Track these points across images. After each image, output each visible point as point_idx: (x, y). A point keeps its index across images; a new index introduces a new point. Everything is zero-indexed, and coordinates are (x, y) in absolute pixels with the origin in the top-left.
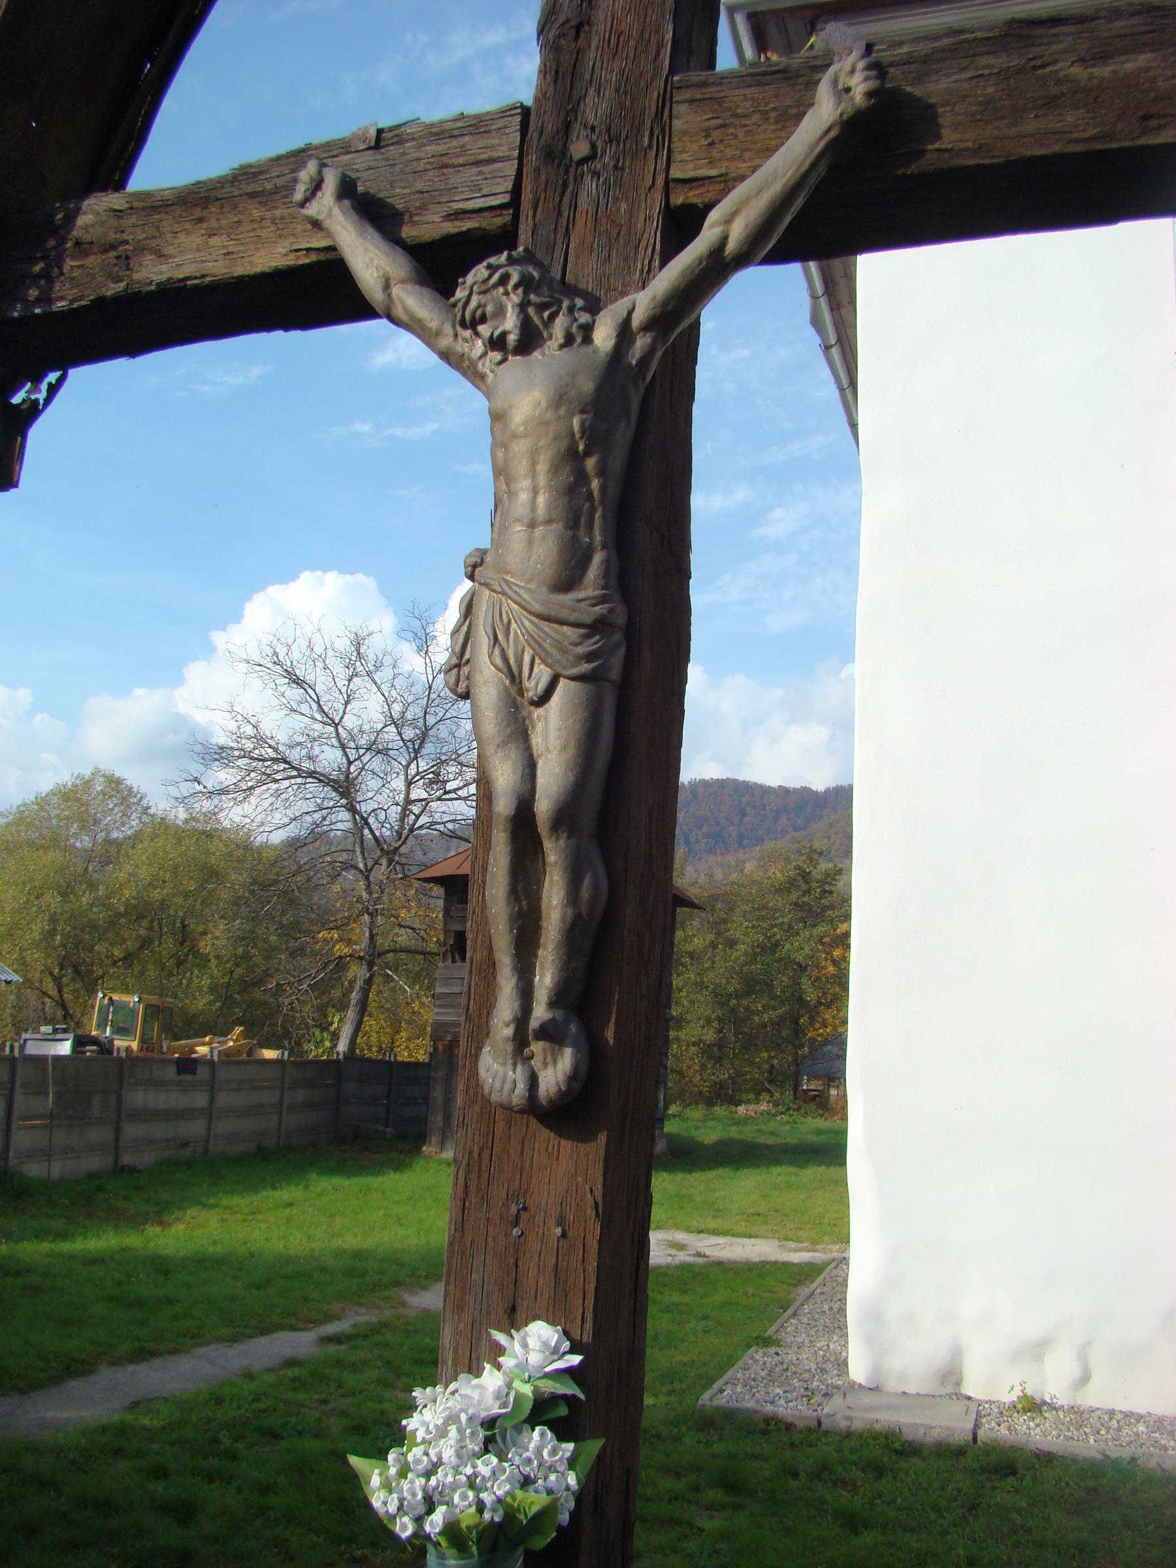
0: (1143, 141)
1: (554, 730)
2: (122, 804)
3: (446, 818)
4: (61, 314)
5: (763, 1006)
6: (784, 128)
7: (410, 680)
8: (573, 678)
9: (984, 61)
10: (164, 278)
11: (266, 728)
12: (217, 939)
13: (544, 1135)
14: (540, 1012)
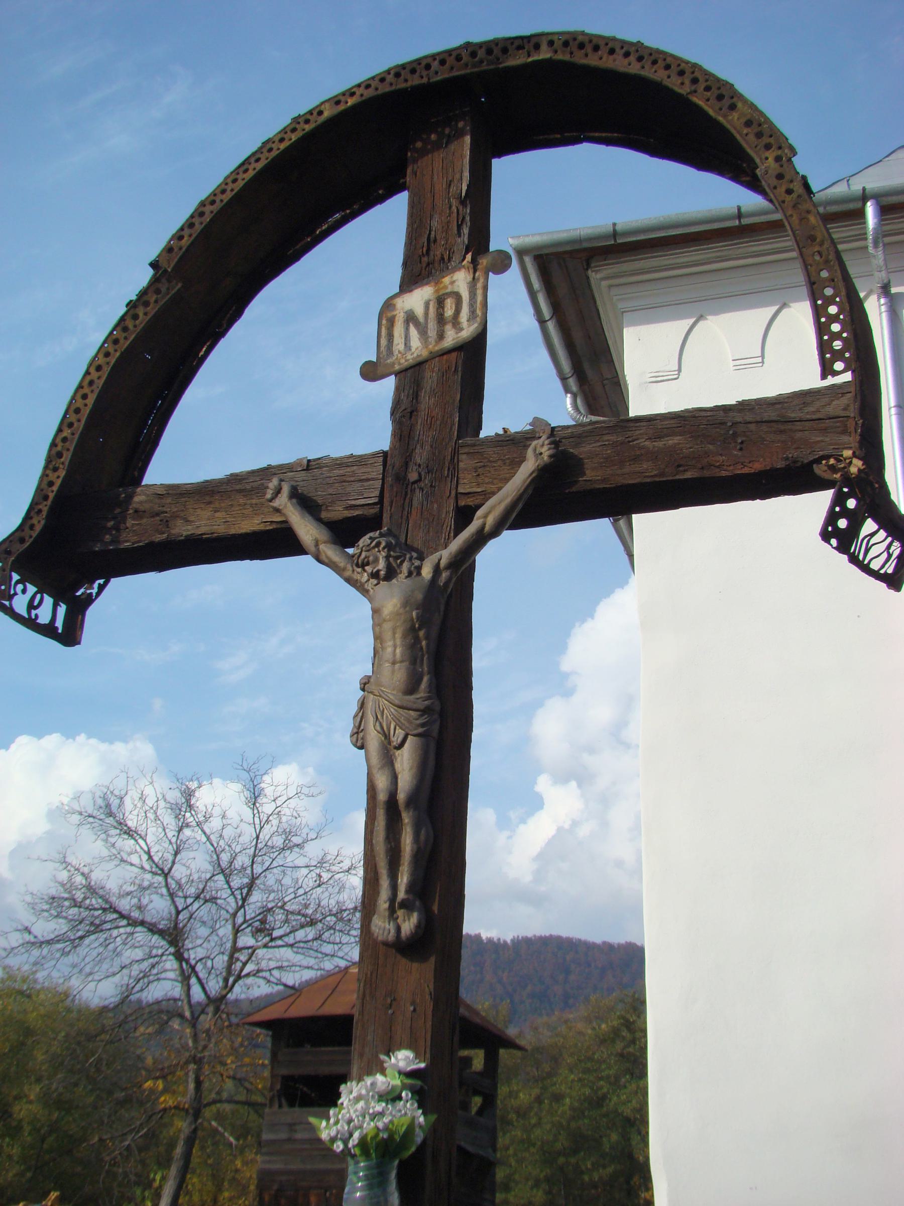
0: (677, 477)
1: (406, 761)
3: (273, 964)
4: (126, 550)
5: (593, 1164)
6: (513, 468)
7: (238, 831)
8: (414, 735)
9: (606, 438)
10: (189, 533)
11: (97, 876)
13: (403, 962)
14: (401, 895)
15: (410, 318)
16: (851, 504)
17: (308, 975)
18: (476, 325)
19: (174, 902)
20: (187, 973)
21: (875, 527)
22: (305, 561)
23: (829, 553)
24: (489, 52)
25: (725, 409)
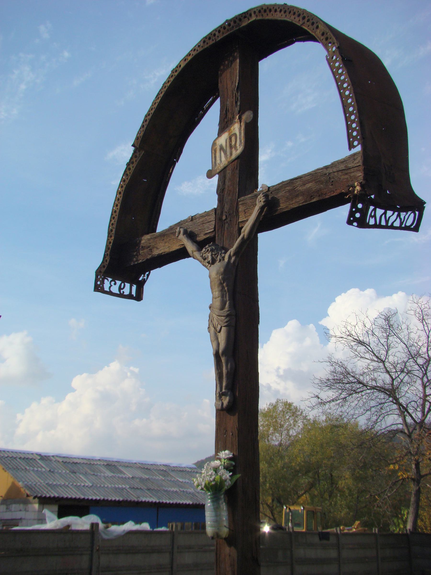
0: (311, 202)
2: (293, 415)
8: (224, 326)
12: (346, 480)
15: (221, 148)
16: (360, 206)
18: (242, 147)
19: (390, 375)
20: (403, 410)
21: (383, 211)
22: (191, 259)
23: (354, 229)
24: (235, 22)
25: (326, 167)
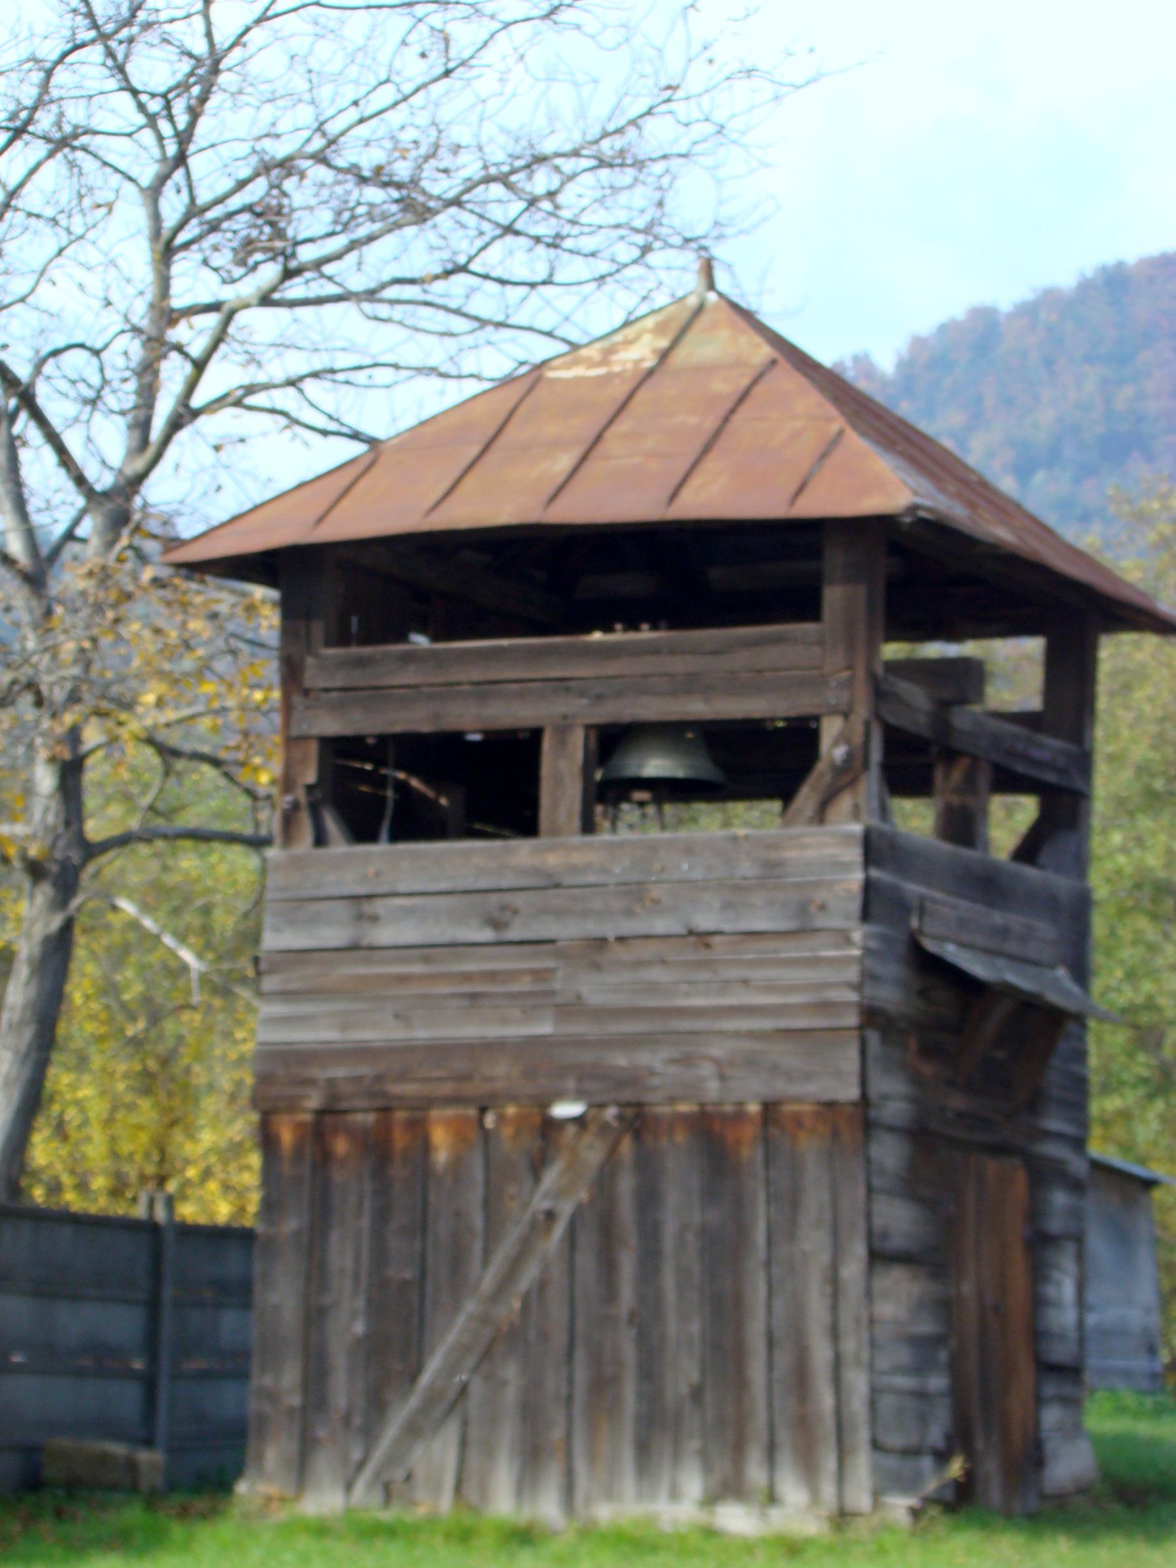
3: (297, 364)
17: (432, 399)
